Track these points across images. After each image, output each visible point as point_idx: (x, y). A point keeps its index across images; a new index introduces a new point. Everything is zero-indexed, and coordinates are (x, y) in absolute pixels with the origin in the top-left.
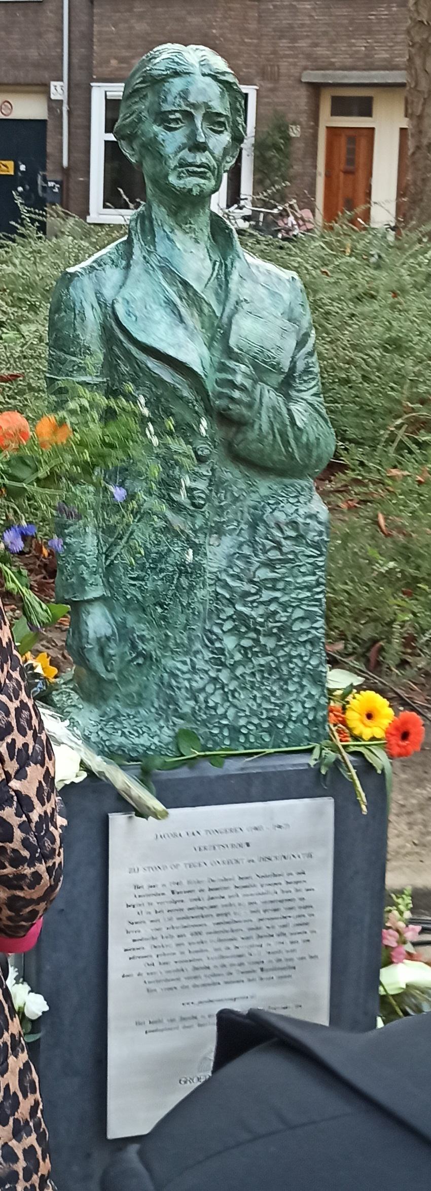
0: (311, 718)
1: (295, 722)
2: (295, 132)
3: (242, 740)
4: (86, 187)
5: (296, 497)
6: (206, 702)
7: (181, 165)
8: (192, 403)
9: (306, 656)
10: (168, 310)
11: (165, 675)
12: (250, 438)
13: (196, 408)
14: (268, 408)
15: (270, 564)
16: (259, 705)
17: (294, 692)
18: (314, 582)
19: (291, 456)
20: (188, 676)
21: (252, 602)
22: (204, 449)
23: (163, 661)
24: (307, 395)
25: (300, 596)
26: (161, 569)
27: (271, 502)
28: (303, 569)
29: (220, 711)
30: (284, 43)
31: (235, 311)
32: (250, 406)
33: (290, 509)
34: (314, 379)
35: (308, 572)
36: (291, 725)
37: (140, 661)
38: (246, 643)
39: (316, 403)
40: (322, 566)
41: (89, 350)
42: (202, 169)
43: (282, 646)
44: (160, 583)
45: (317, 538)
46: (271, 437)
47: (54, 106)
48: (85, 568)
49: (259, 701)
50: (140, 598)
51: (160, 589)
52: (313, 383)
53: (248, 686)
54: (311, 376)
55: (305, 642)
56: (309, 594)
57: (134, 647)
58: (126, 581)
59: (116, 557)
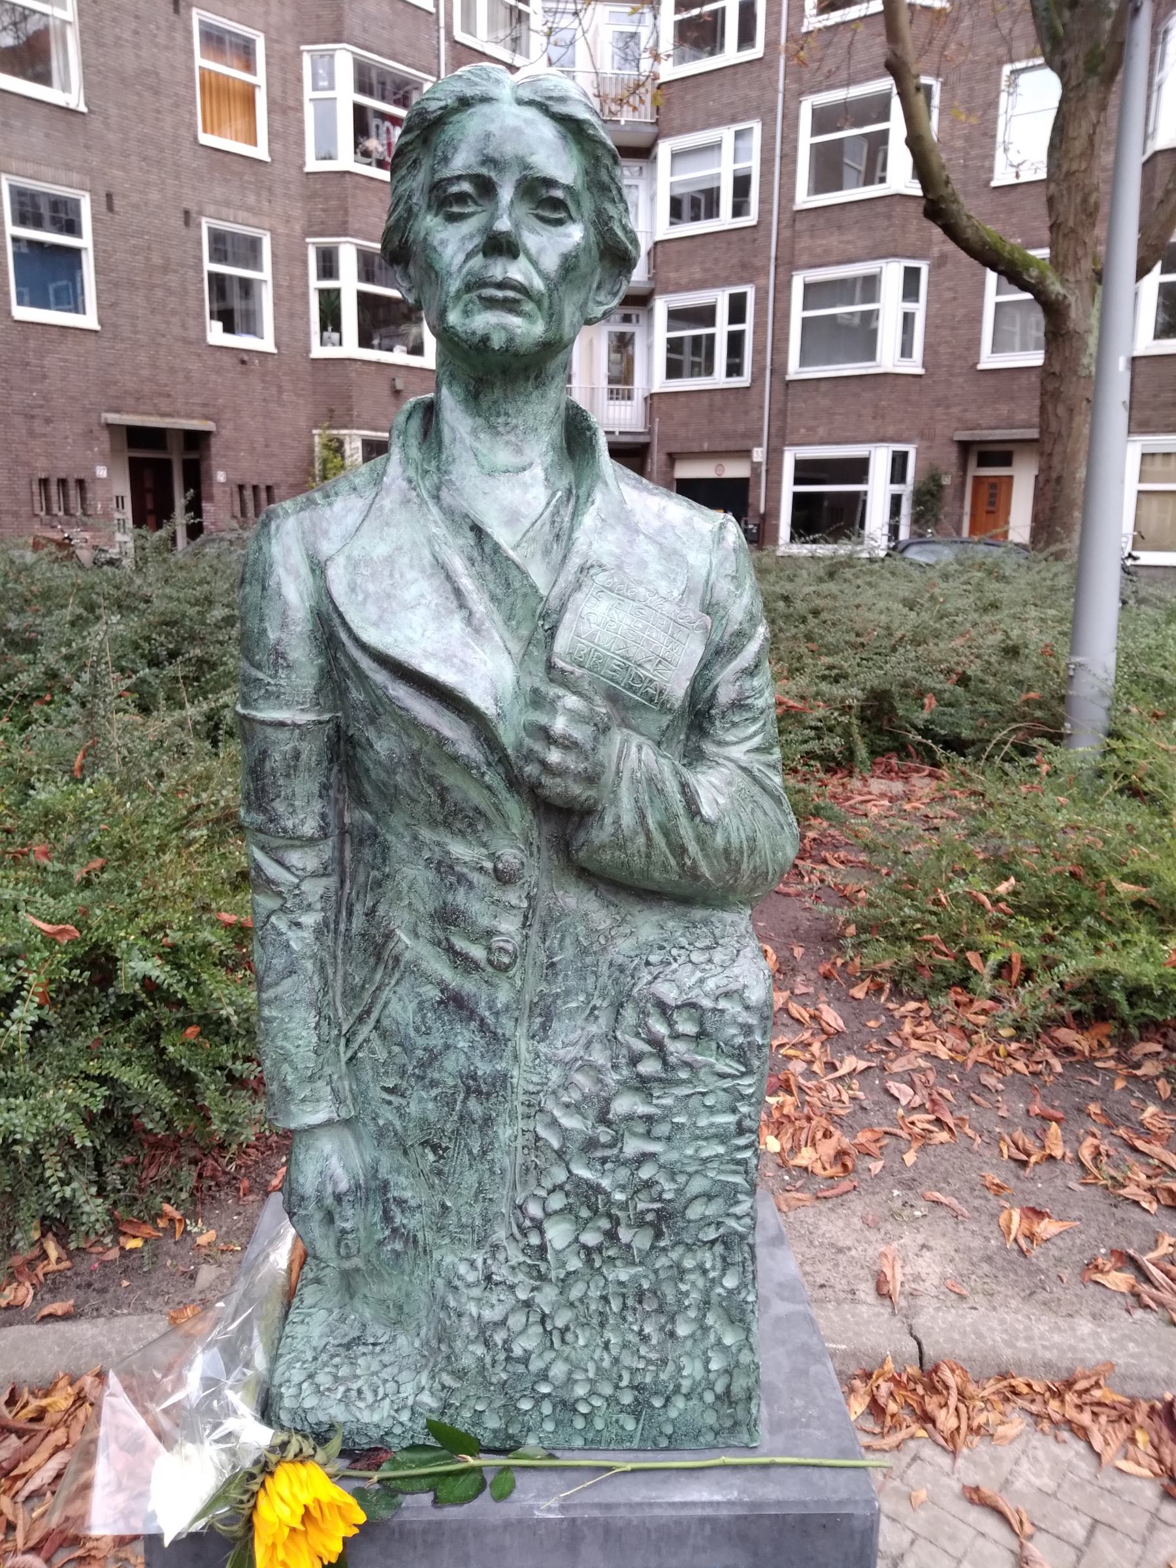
0: (720, 1388)
1: (688, 1397)
2: (946, 481)
3: (579, 1423)
4: (776, 528)
5: (708, 948)
6: (509, 1350)
7: (469, 287)
8: (478, 768)
9: (713, 1268)
10: (436, 582)
11: (440, 1282)
12: (597, 842)
13: (487, 778)
14: (635, 781)
15: (643, 1086)
16: (616, 1361)
17: (686, 1338)
18: (733, 1127)
19: (695, 875)
20: (476, 1292)
21: (604, 1161)
22: (510, 855)
23: (437, 1255)
24: (737, 752)
25: (705, 1154)
26: (432, 1081)
27: (653, 958)
28: (710, 1101)
29: (536, 1365)
30: (939, 410)
31: (578, 586)
32: (591, 779)
33: (688, 976)
34: (754, 720)
35: (719, 1106)
36: (680, 1402)
37: (398, 1246)
38: (591, 1238)
39: (756, 767)
40: (751, 1096)
41: (285, 659)
42: (511, 294)
43: (664, 1249)
44: (431, 1105)
45: (740, 1040)
46: (641, 840)
47: (755, 467)
48: (290, 1070)
49: (615, 1351)
50: (399, 1128)
51: (432, 1118)
52: (753, 729)
53: (595, 1321)
54: (749, 715)
55: (713, 1242)
56: (721, 1150)
57: (387, 1218)
58: (376, 1093)
59: (361, 1047)
